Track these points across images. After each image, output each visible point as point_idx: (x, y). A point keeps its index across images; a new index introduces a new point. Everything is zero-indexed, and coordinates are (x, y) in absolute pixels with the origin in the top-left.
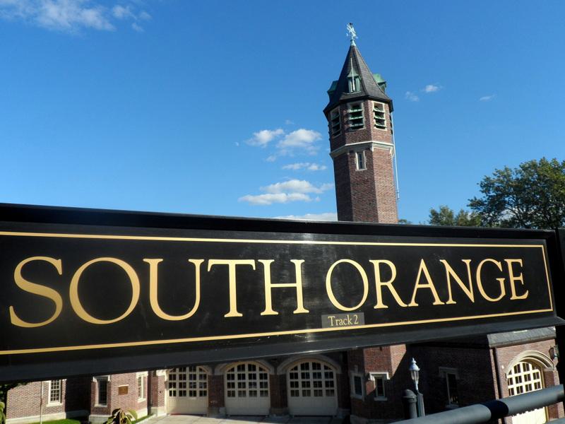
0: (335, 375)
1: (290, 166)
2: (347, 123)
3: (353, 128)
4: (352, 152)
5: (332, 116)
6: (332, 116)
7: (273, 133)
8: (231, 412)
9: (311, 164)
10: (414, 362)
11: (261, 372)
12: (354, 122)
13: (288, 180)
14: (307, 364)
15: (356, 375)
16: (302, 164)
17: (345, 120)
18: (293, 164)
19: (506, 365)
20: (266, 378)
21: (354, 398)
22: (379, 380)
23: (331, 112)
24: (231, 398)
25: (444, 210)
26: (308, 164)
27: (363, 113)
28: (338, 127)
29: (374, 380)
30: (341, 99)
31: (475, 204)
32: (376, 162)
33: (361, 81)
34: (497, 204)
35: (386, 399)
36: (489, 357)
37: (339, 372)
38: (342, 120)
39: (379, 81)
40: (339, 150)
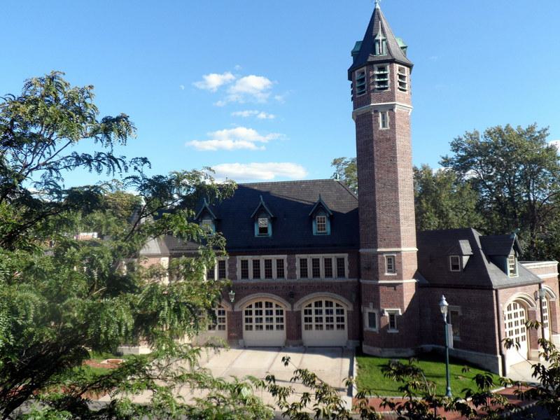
0: (284, 313)
1: (239, 113)
2: (373, 84)
3: (379, 89)
4: (376, 112)
5: (357, 76)
6: (356, 76)
7: (222, 77)
8: (248, 344)
9: (260, 112)
10: (444, 298)
11: (338, 308)
12: (380, 83)
13: (235, 128)
14: (321, 302)
15: (371, 311)
16: (251, 112)
17: (371, 81)
18: (243, 111)
19: (503, 304)
20: (282, 314)
21: (367, 331)
22: (392, 316)
23: (356, 72)
24: (249, 331)
25: (424, 168)
26: (256, 112)
27: (388, 75)
28: (363, 87)
29: (388, 315)
30: (369, 60)
31: (446, 162)
32: (398, 123)
33: (387, 44)
34: (464, 164)
35: (397, 331)
36: (492, 297)
37: (351, 308)
38: (368, 80)
39: (401, 45)
40: (363, 109)
